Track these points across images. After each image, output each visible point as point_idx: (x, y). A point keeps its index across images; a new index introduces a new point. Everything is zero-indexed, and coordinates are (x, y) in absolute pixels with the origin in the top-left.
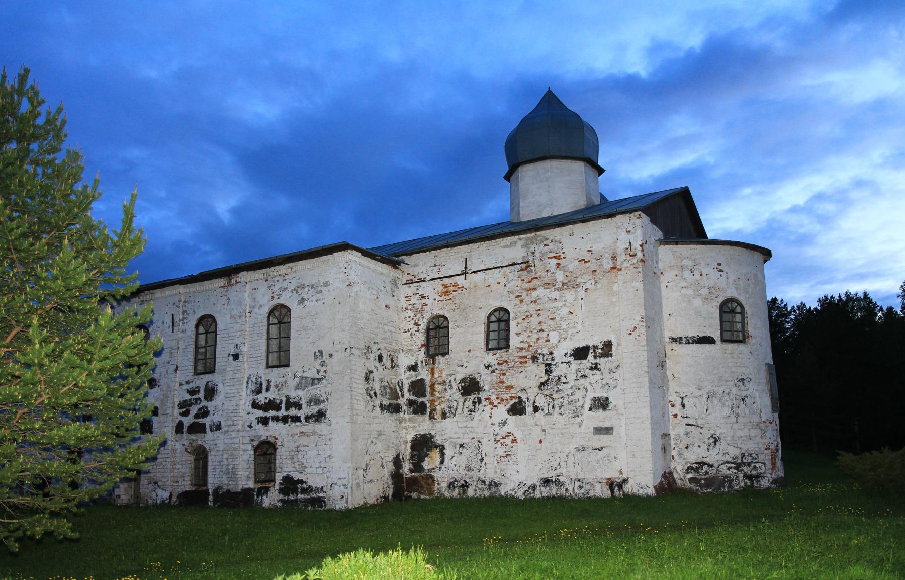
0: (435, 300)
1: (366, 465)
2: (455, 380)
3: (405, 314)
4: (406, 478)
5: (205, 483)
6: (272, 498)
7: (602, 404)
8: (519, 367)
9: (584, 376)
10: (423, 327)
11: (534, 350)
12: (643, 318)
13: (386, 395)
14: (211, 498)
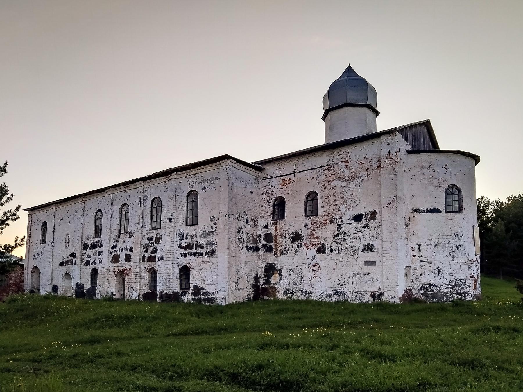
0: (278, 188)
1: (238, 280)
3: (261, 197)
5: (155, 286)
6: (188, 298)
7: (369, 248)
8: (322, 226)
9: (360, 231)
10: (272, 204)
11: (331, 216)
13: (250, 241)
14: (158, 296)
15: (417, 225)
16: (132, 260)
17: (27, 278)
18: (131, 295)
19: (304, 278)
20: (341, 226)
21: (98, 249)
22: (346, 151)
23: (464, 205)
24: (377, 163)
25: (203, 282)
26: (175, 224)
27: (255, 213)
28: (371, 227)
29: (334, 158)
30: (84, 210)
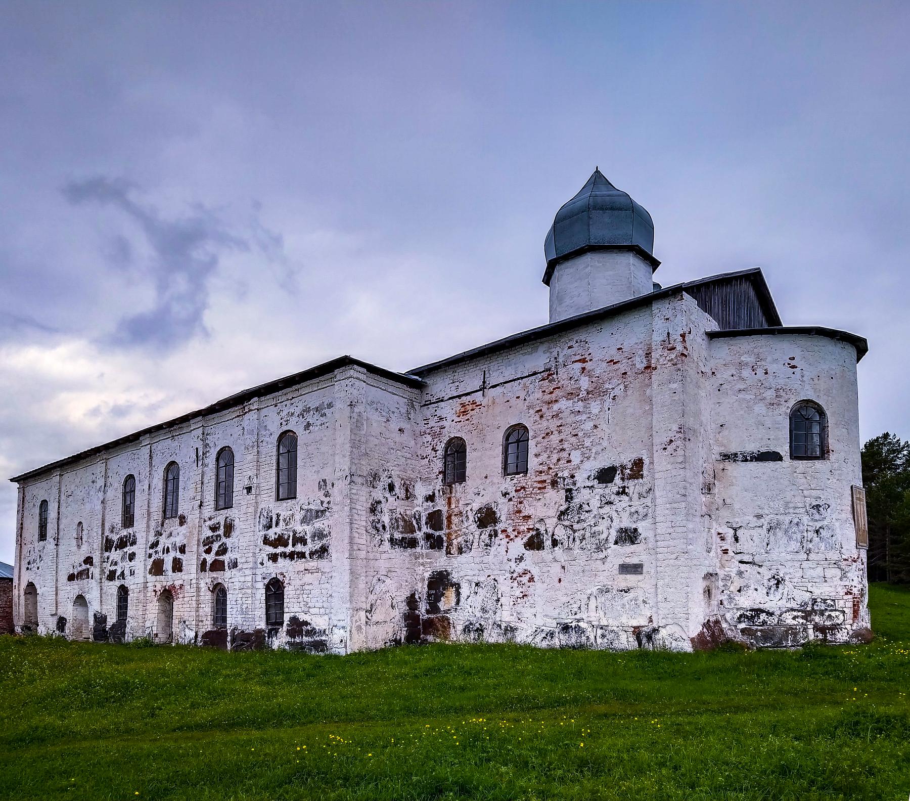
0: (453, 421)
1: (372, 605)
2: (471, 510)
4: (423, 619)
5: (224, 620)
6: (280, 641)
7: (629, 536)
8: (536, 494)
10: (440, 453)
11: (554, 474)
12: (681, 428)
13: (398, 527)
14: (229, 638)
15: (731, 487)
16: (184, 568)
17: (19, 604)
18: (183, 636)
19: (502, 600)
20: (572, 494)
21: (129, 549)
22: (583, 338)
23: (832, 442)
24: (645, 361)
25: (306, 609)
26: (256, 497)
27: (409, 472)
28: (633, 493)
29: (558, 355)
30: (106, 477)
